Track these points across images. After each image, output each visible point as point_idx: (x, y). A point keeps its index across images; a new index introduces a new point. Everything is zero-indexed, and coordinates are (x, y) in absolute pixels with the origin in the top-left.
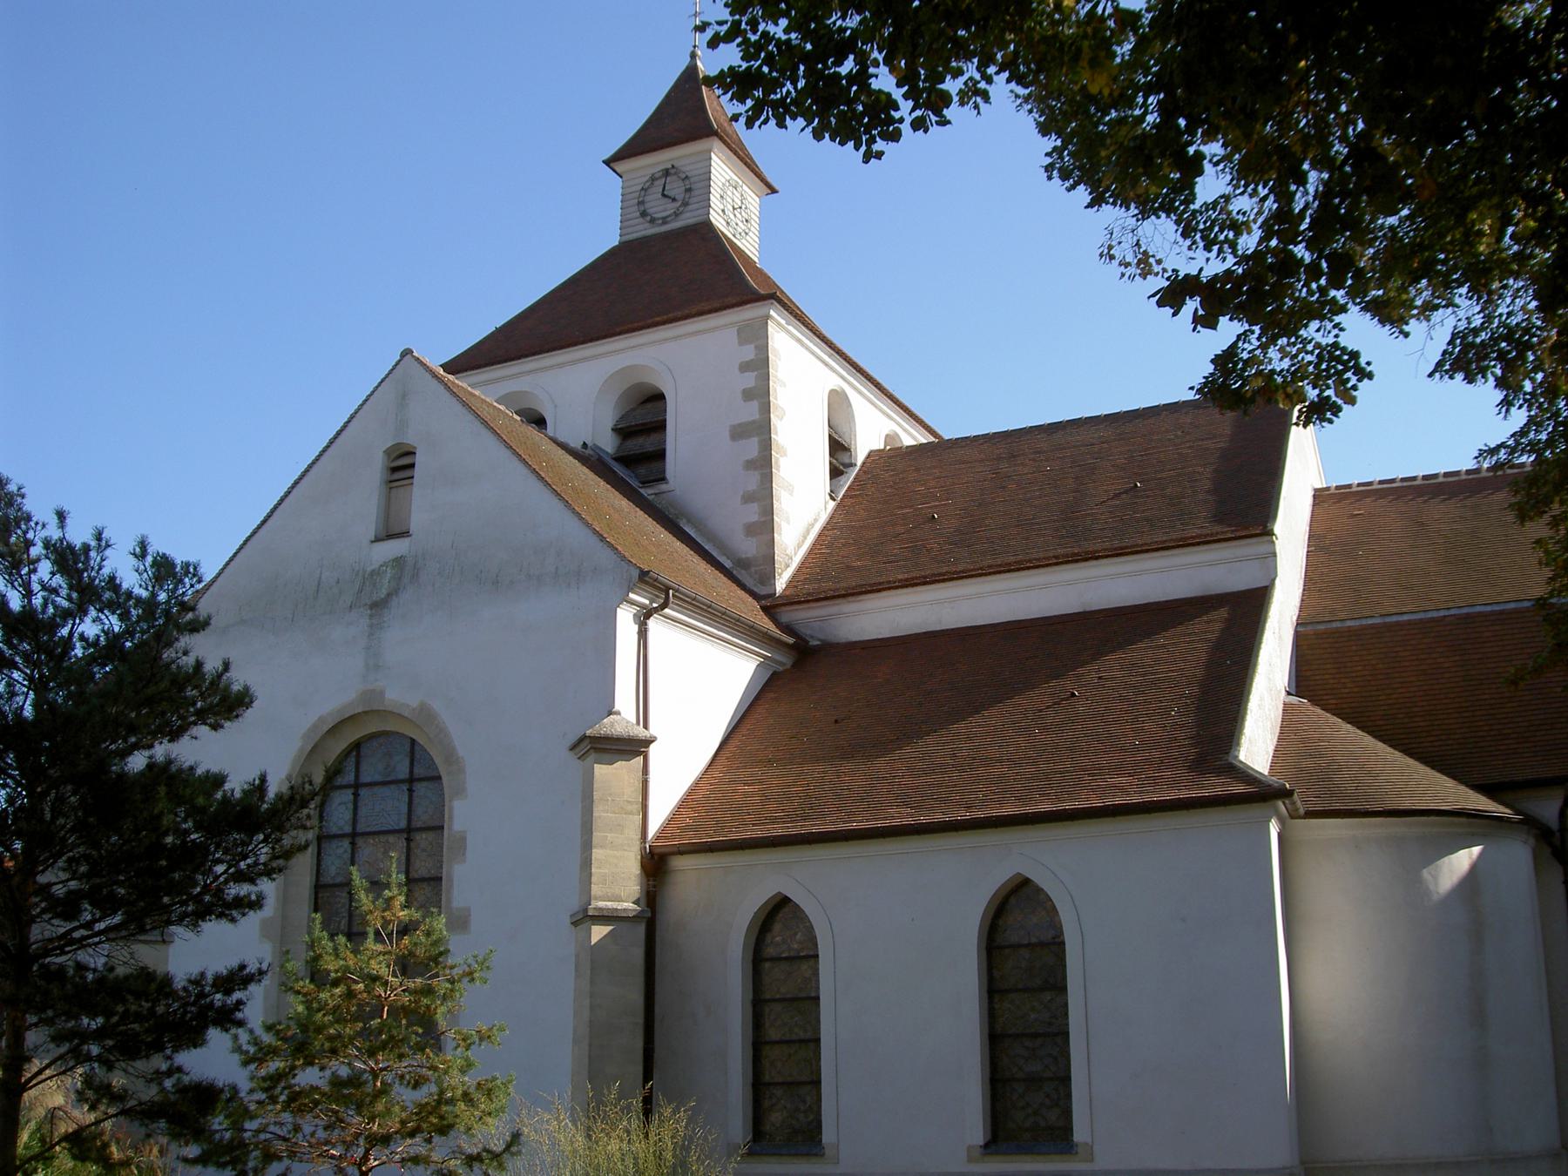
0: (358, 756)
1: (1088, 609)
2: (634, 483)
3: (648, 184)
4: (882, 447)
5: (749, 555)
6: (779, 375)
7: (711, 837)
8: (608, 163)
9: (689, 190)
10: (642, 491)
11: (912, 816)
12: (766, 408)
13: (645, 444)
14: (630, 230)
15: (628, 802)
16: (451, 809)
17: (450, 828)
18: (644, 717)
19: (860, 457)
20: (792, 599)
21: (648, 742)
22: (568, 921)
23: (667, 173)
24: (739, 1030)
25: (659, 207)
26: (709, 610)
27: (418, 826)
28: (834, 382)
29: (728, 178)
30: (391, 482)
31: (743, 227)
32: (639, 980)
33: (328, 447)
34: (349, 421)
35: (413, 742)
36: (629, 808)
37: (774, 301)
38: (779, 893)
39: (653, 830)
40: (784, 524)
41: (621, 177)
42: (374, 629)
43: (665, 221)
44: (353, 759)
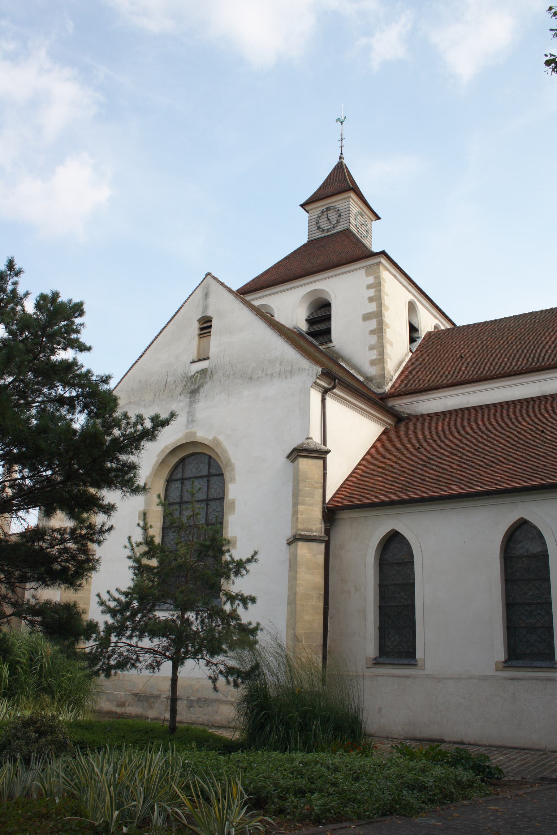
0: (183, 465)
1: (544, 394)
2: (317, 344)
3: (320, 215)
4: (433, 330)
5: (372, 375)
6: (386, 291)
7: (358, 501)
8: (302, 206)
9: (340, 216)
10: (320, 347)
11: (463, 489)
12: (380, 305)
13: (322, 326)
14: (312, 236)
15: (316, 482)
16: (228, 489)
17: (227, 498)
18: (324, 442)
19: (423, 334)
20: (395, 394)
21: (328, 452)
22: (285, 542)
23: (328, 209)
24: (372, 599)
25: (324, 224)
27: (212, 498)
28: (410, 297)
29: (358, 211)
31: (365, 234)
32: (322, 572)
33: (171, 320)
34: (181, 308)
35: (210, 456)
36: (317, 485)
37: (383, 255)
38: (393, 530)
39: (328, 497)
40: (388, 360)
41: (308, 213)
42: (192, 403)
43: (328, 230)
44: (181, 467)
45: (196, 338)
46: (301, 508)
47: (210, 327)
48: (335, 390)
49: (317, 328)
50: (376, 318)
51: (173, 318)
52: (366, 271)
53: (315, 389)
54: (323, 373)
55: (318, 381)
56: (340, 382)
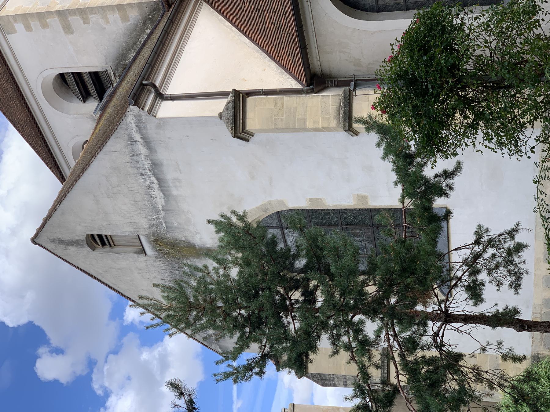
10: (115, 85)
15: (275, 105)
26: (158, 53)
30: (110, 246)
36: (279, 104)
39: (293, 84)
45: (116, 249)
46: (309, 125)
47: (100, 236)
48: (157, 84)
49: (92, 89)
50: (67, 18)
51: (95, 278)
52: (9, 34)
53: (157, 111)
54: (136, 104)
55: (147, 108)
56: (146, 78)
